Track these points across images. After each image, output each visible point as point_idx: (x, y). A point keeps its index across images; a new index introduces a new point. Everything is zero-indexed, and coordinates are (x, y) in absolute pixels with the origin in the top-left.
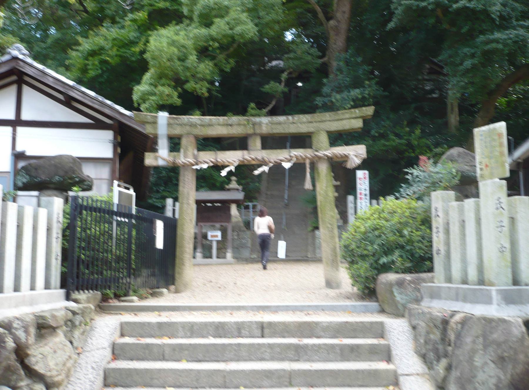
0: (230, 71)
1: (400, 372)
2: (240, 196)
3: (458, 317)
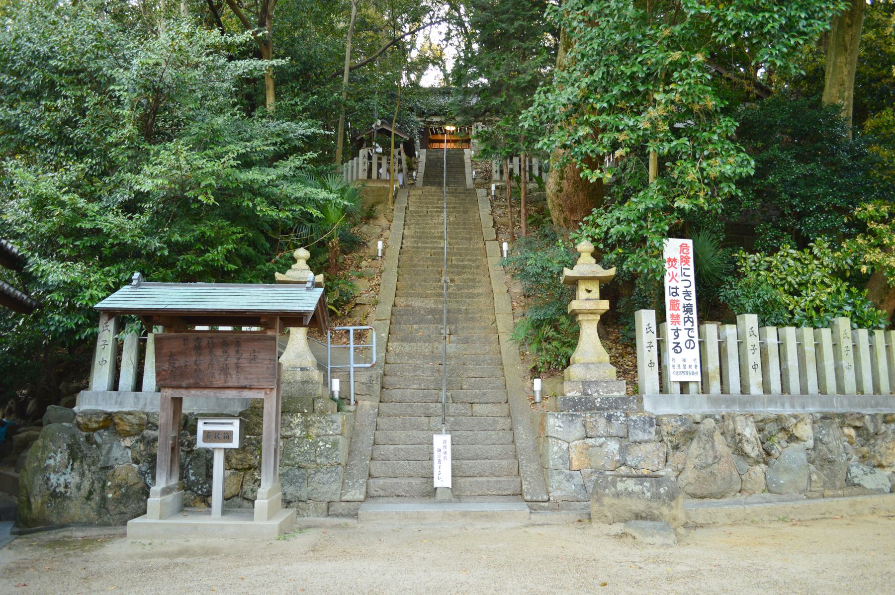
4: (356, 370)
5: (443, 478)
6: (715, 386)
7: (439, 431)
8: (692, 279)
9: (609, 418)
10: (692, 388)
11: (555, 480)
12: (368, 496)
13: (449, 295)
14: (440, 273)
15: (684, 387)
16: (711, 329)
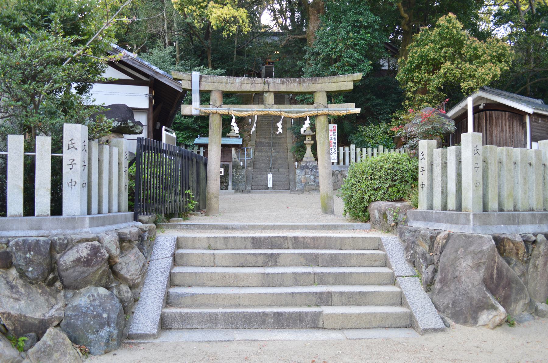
0: (480, 30)
1: (396, 274)
2: (239, 141)
3: (442, 235)
4: (247, 159)
5: (270, 184)
6: (341, 163)
7: (269, 174)
8: (336, 135)
9: (311, 170)
10: (335, 164)
11: (298, 185)
12: (252, 189)
13: (273, 138)
14: (270, 130)
15: (333, 163)
16: (341, 149)
